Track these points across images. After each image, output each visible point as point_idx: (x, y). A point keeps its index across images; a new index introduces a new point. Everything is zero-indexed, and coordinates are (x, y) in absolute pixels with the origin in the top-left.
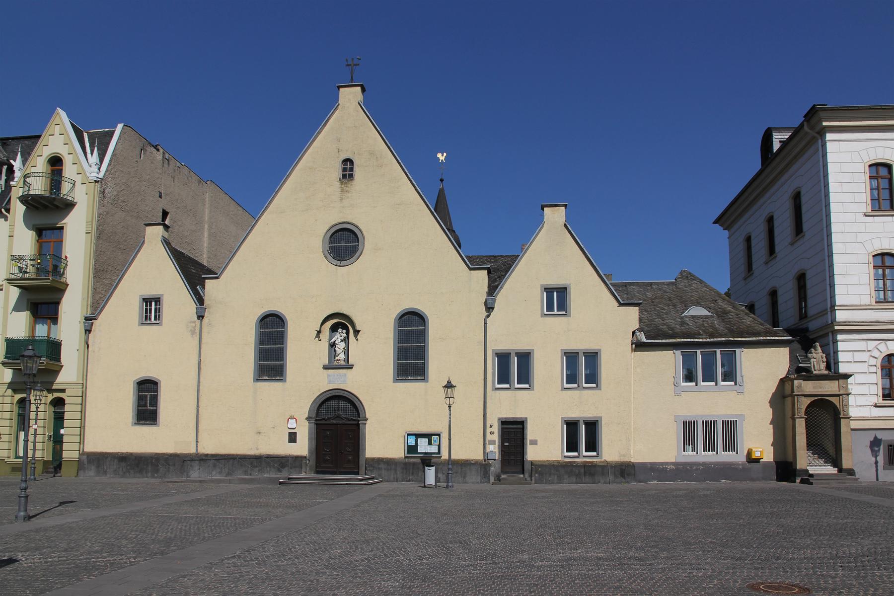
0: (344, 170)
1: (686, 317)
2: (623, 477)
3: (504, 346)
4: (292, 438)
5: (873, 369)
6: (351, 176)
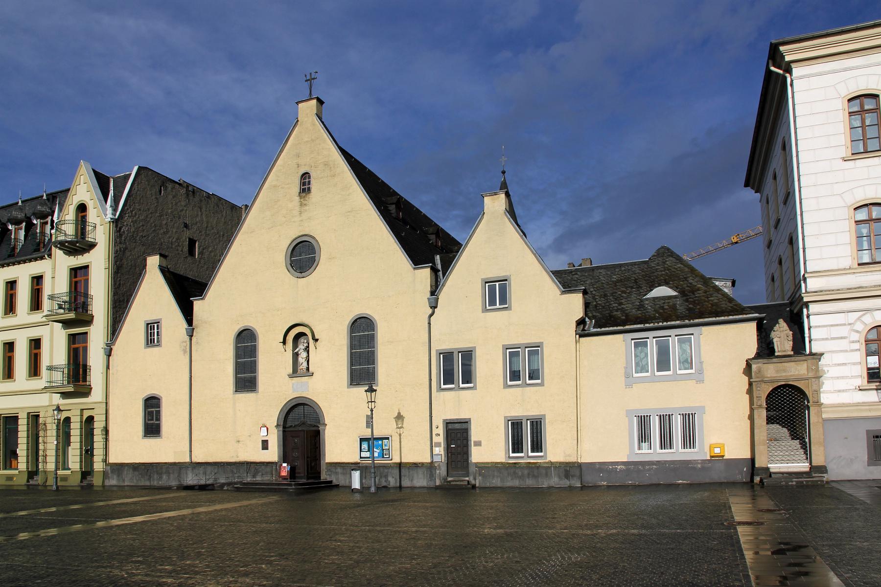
0: (304, 184)
1: (647, 299)
2: (567, 479)
3: (446, 346)
4: (265, 445)
5: (856, 346)
6: (309, 189)
